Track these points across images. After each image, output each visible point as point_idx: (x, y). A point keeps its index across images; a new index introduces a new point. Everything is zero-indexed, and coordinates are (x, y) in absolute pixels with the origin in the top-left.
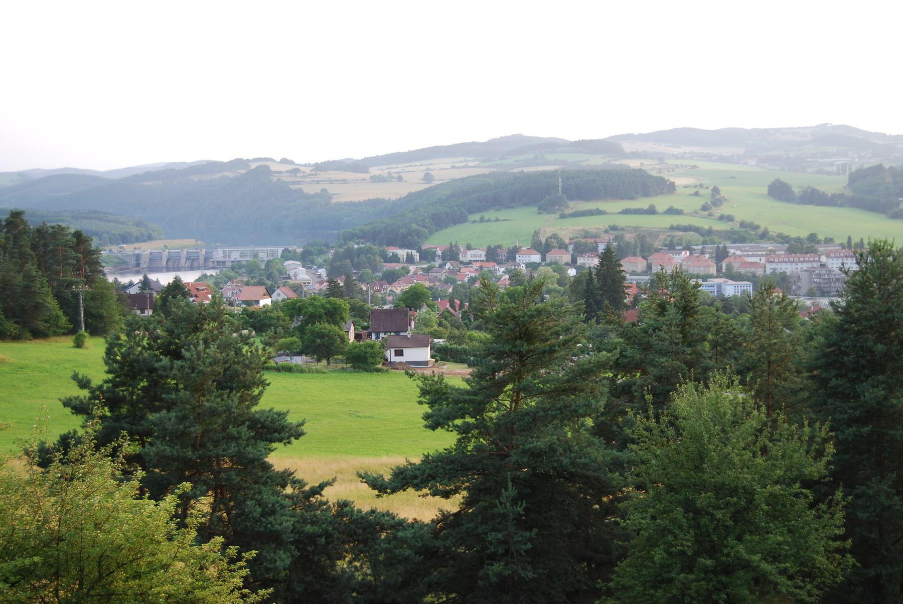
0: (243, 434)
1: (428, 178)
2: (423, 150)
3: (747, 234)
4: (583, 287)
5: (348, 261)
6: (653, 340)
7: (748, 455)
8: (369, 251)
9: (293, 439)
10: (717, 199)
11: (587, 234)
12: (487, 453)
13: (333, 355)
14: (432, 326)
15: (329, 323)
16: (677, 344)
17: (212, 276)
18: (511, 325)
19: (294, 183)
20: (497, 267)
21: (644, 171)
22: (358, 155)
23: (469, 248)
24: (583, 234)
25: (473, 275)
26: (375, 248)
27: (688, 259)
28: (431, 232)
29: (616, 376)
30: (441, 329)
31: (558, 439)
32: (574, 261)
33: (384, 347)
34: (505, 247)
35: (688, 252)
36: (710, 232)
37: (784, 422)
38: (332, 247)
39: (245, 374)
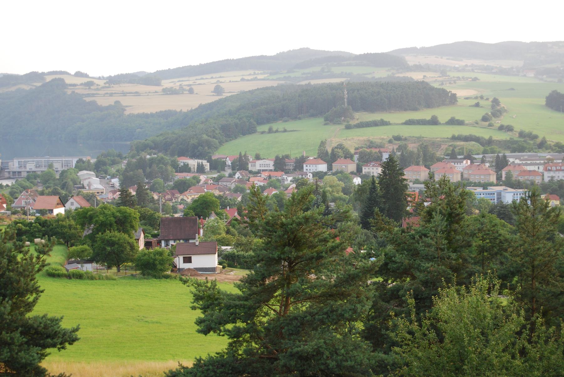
0: (16, 341)
1: (218, 90)
2: (213, 63)
3: (526, 143)
4: (366, 195)
5: (141, 171)
6: (420, 246)
7: (507, 357)
8: (161, 161)
9: (67, 344)
10: (497, 110)
11: (371, 145)
12: (257, 357)
13: (124, 262)
14: (220, 234)
15: (120, 232)
16: (442, 250)
17: (7, 186)
18: (280, 232)
19: (88, 95)
20: (285, 177)
21: (427, 84)
22: (151, 68)
23: (258, 158)
24: (368, 144)
25: (262, 184)
26: (167, 158)
27: (469, 167)
28: (221, 143)
29: (386, 281)
30: (229, 236)
31: (325, 343)
32: (359, 171)
33: (172, 254)
34: (293, 157)
35: (469, 161)
36: (490, 142)
37: (542, 325)
38: (125, 158)
39: (18, 282)
